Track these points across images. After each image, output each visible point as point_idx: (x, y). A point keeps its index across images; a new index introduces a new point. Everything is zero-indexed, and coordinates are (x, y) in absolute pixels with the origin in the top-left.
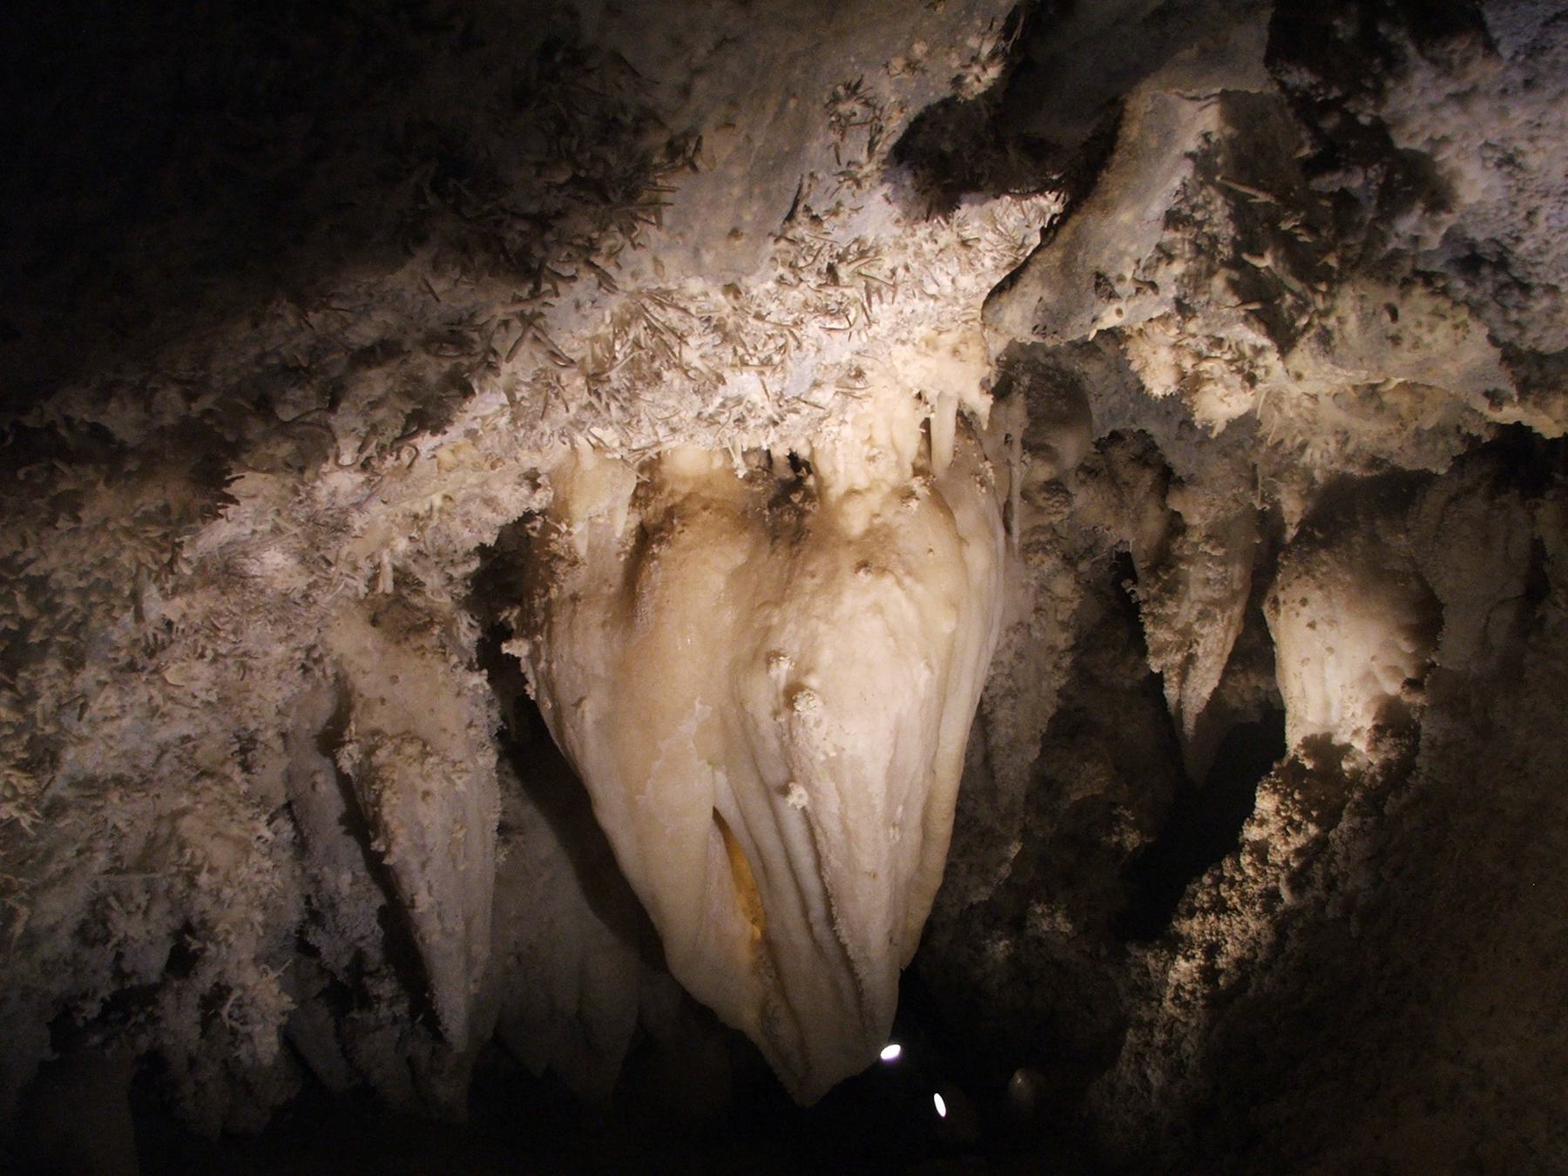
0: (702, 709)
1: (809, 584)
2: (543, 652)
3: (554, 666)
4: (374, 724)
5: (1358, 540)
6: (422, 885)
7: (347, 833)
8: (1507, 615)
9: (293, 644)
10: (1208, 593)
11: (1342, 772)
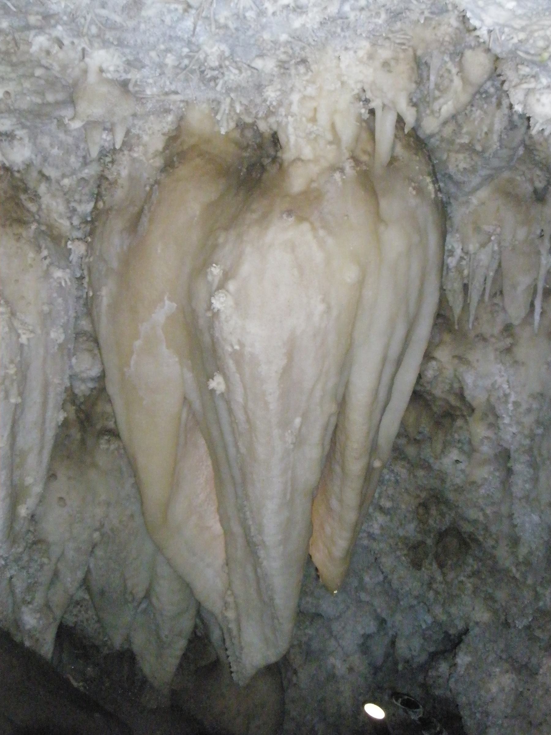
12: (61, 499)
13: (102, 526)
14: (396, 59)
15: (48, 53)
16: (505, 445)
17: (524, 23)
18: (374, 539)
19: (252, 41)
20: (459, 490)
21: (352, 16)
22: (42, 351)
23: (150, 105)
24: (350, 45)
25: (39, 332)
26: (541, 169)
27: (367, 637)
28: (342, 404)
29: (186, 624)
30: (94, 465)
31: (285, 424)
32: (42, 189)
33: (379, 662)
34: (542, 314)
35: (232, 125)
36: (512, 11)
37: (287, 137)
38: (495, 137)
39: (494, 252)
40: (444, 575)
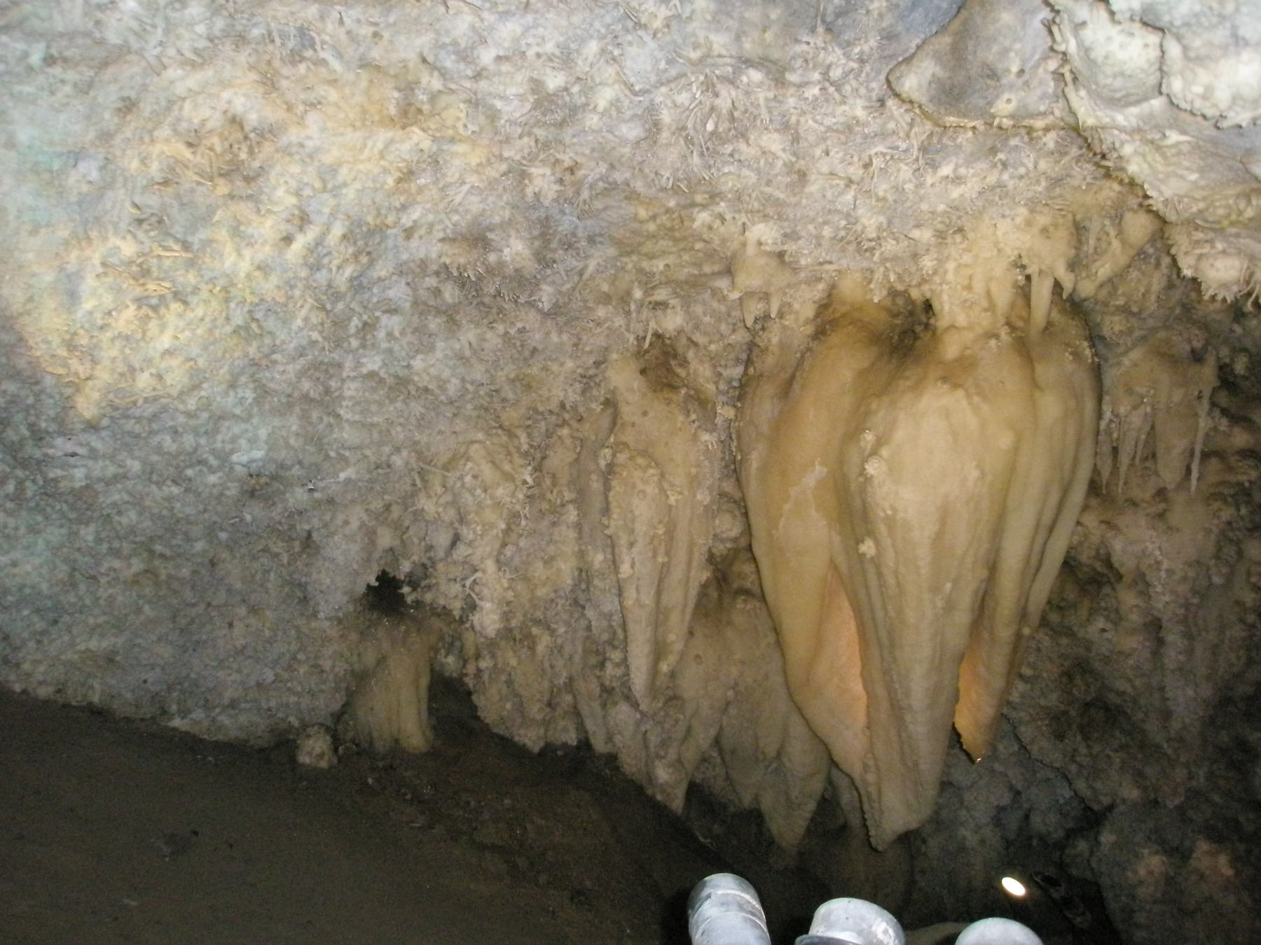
4: (624, 438)
9: (578, 363)
12: (698, 656)
13: (736, 684)
14: (1056, 226)
15: (710, 228)
16: (1156, 613)
17: (1205, 193)
18: (1015, 709)
19: (910, 212)
20: (1106, 660)
21: (1011, 184)
22: (688, 512)
23: (803, 275)
24: (1007, 212)
25: (686, 493)
26: (1200, 328)
27: (1001, 809)
28: (993, 568)
29: (817, 786)
30: (730, 623)
31: (935, 589)
32: (690, 354)
33: (1012, 836)
34: (1199, 479)
35: (885, 293)
36: (1195, 183)
37: (941, 303)
38: (1153, 298)
39: (1146, 414)
40: (1089, 747)
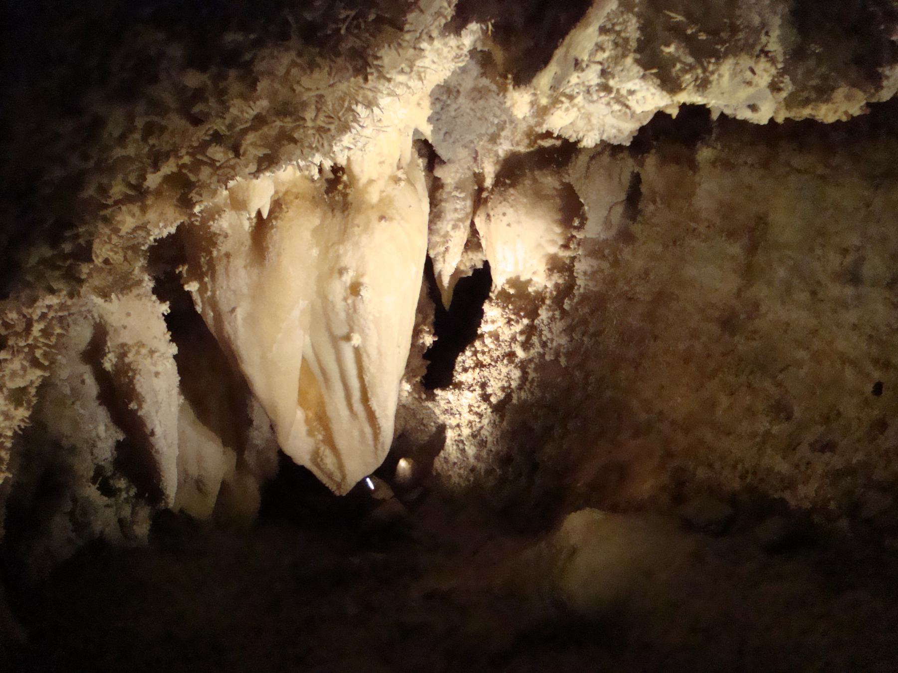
0: (303, 304)
1: (356, 229)
2: (209, 287)
3: (218, 292)
4: (121, 340)
5: (528, 182)
6: (157, 422)
7: (100, 404)
8: (619, 210)
10: (457, 216)
11: (530, 293)
